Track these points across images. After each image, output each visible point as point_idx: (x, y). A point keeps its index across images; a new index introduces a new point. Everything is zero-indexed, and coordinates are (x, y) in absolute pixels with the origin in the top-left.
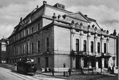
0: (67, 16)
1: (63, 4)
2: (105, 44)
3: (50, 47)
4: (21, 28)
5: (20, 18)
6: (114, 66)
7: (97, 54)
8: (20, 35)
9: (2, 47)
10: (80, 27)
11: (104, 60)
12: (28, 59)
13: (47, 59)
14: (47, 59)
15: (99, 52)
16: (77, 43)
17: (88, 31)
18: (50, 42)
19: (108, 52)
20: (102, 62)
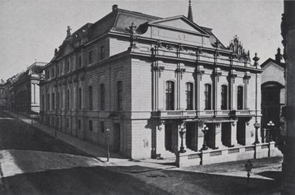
0: (151, 26)
1: (30, 64)
2: (240, 89)
3: (124, 103)
4: (67, 51)
5: (67, 29)
6: (257, 141)
7: (220, 113)
8: (65, 63)
9: (32, 85)
10: (177, 53)
11: (236, 126)
12: (84, 31)
13: (117, 126)
14: (117, 126)
15: (224, 107)
16: (189, 90)
17: (231, 65)
18: (123, 89)
19: (248, 107)
20: (232, 130)
